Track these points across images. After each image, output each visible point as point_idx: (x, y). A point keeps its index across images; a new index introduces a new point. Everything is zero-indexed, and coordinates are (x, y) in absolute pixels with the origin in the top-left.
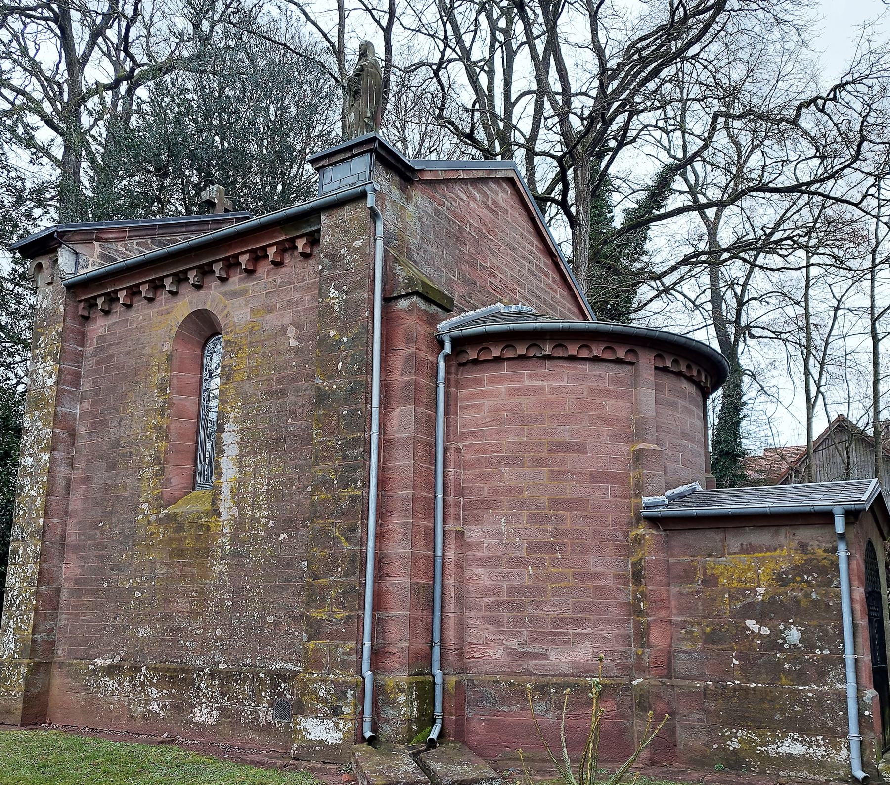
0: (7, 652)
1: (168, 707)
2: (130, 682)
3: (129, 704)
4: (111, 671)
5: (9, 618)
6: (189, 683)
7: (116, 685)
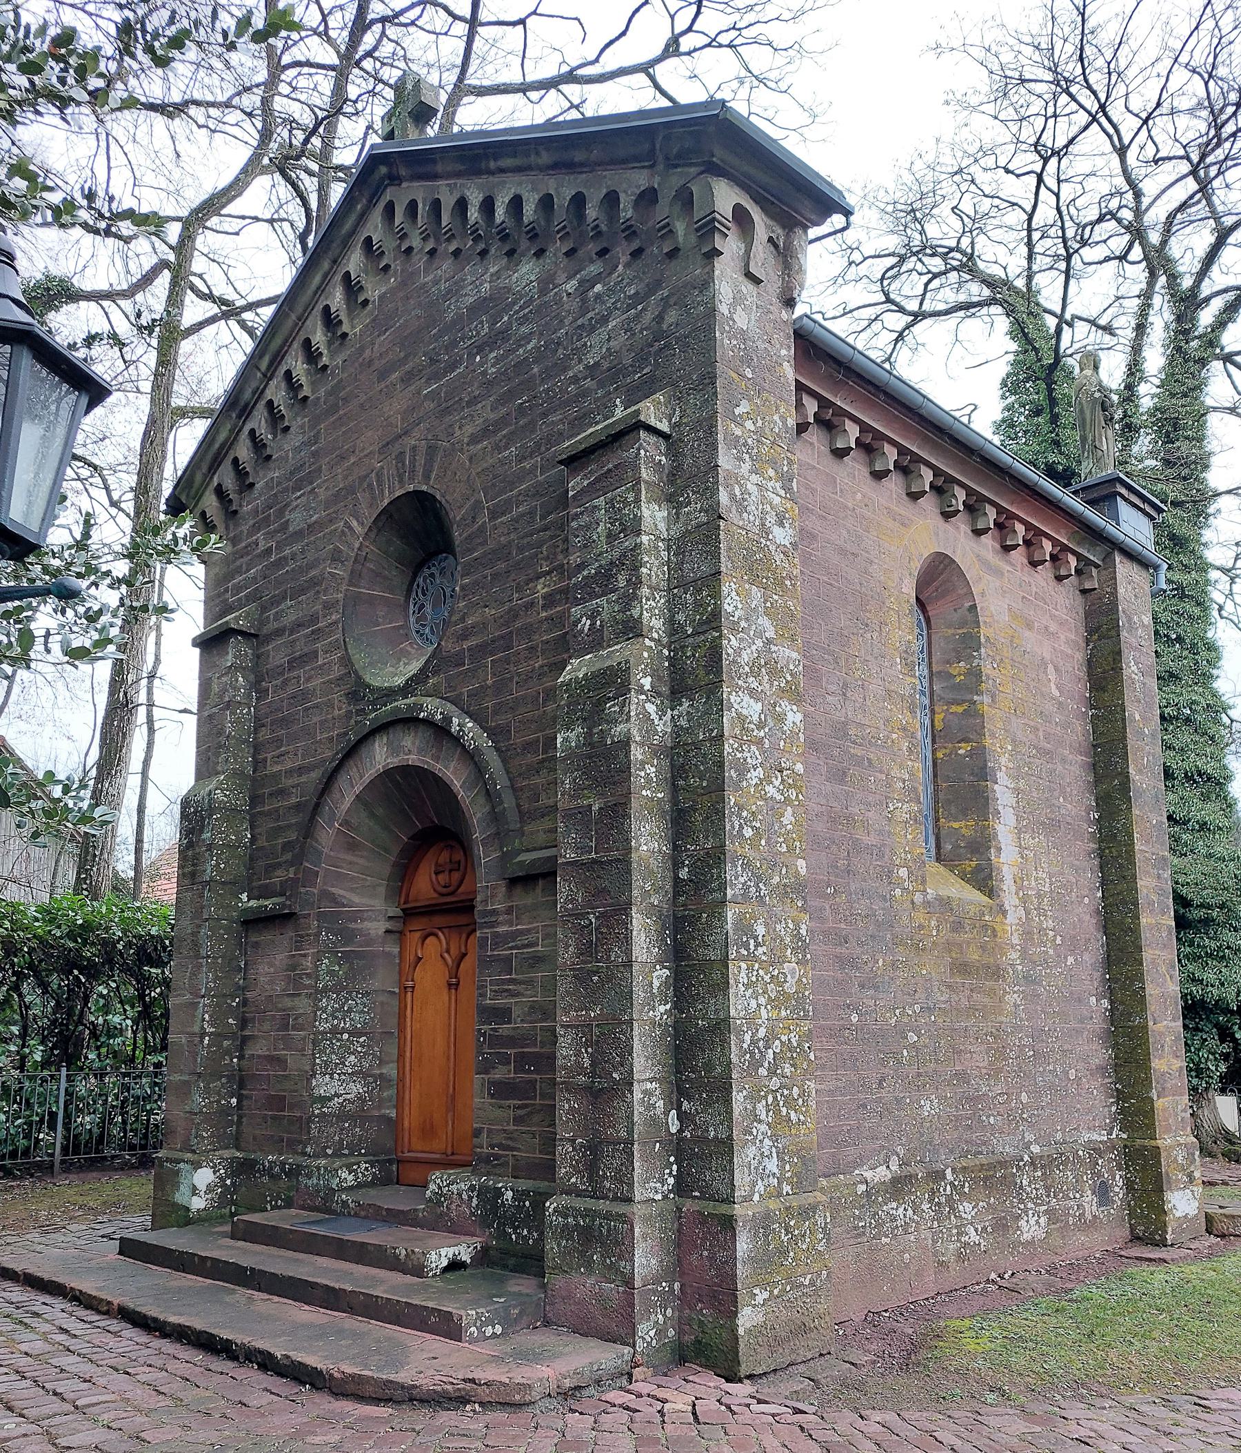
0: (760, 1186)
1: (989, 1229)
2: (931, 1201)
3: (935, 1242)
4: (898, 1187)
5: (754, 1098)
6: (1009, 1183)
7: (910, 1212)
